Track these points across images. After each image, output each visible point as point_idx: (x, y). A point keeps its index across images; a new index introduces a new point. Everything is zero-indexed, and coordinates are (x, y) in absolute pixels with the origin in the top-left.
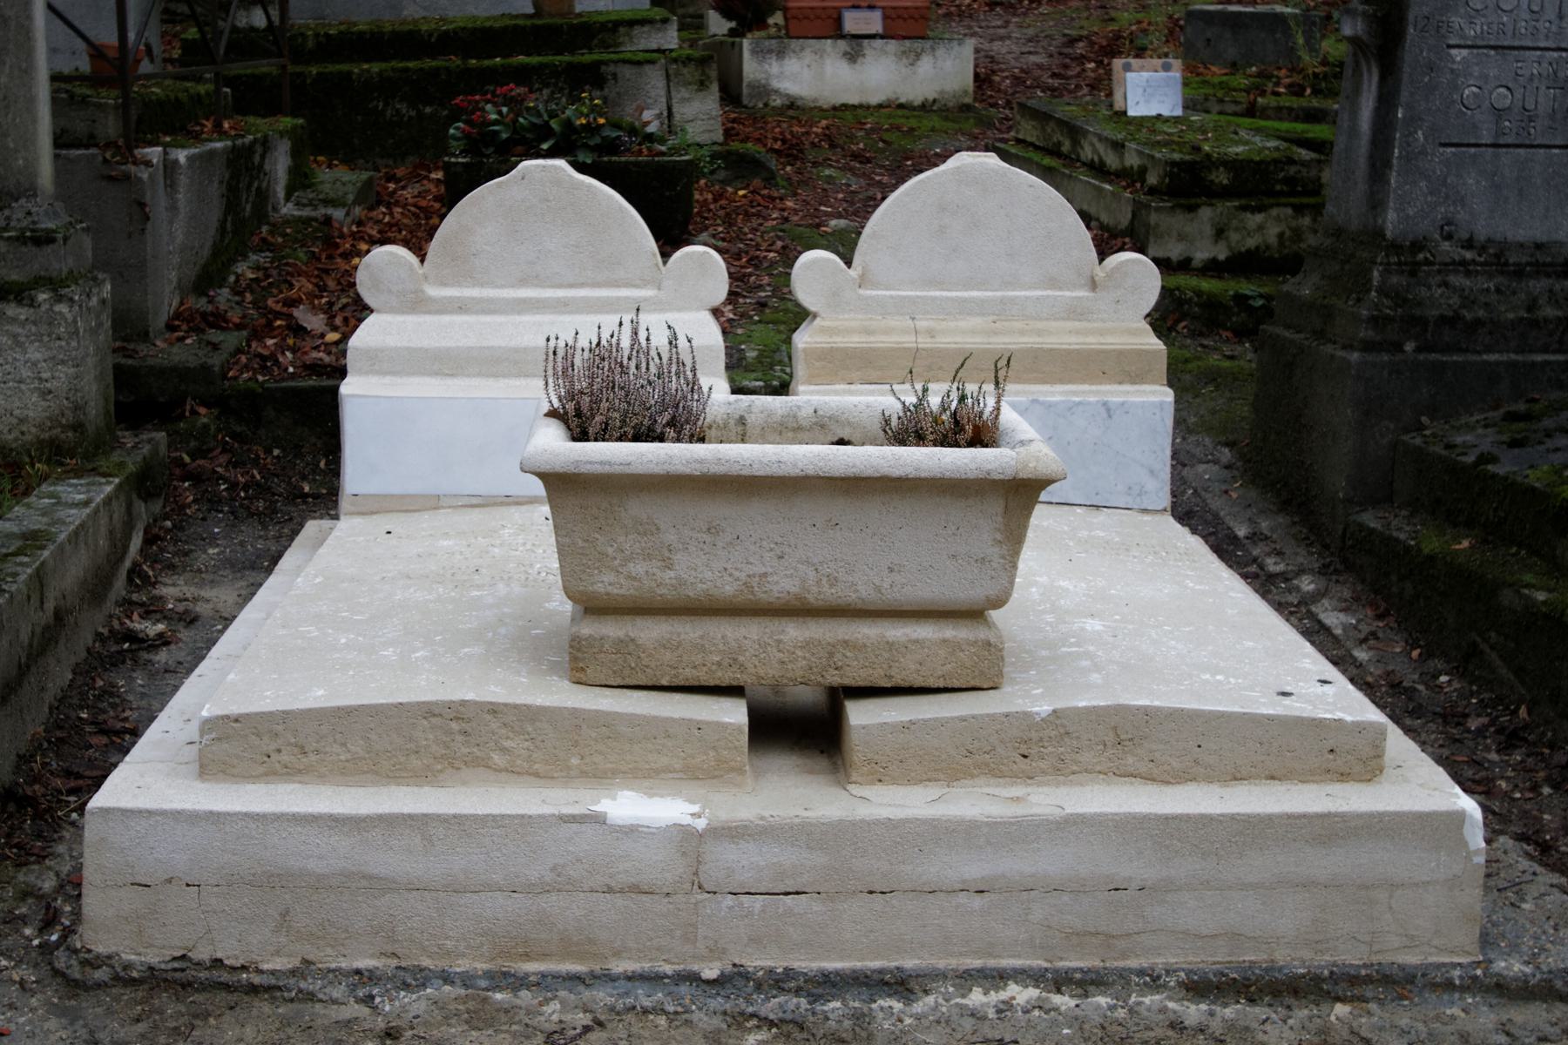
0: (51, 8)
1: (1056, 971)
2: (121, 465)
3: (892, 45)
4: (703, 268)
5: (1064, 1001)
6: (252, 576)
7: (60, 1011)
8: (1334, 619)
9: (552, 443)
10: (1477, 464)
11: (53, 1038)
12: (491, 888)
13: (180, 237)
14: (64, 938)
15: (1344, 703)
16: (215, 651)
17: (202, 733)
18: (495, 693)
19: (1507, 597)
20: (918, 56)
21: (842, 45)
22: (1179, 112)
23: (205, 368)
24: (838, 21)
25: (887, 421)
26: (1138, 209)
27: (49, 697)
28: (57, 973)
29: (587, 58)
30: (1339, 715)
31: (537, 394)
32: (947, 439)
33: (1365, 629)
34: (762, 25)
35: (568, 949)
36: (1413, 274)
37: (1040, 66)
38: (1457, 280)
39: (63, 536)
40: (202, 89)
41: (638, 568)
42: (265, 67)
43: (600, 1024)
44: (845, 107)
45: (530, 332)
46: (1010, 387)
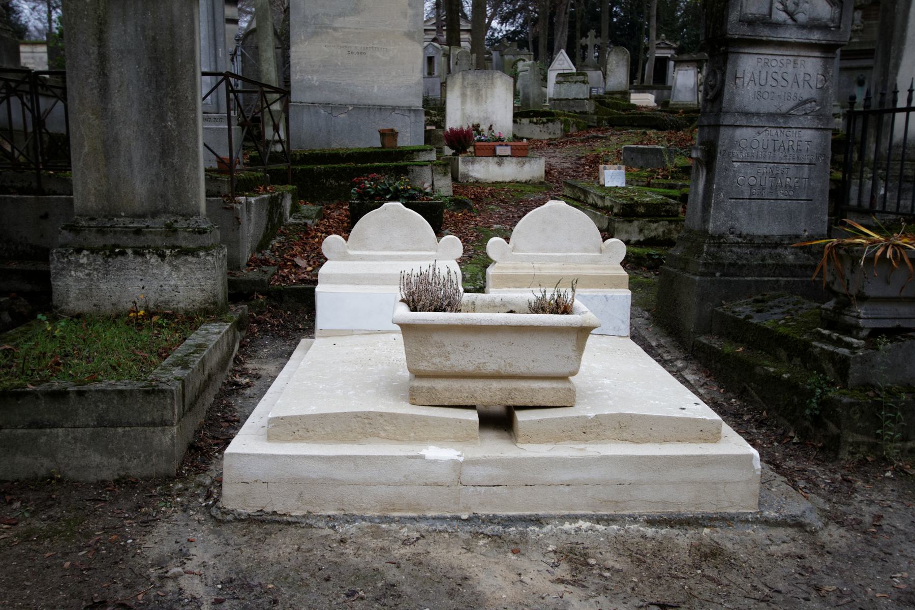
0: (205, 145)
1: (597, 515)
2: (231, 318)
3: (514, 159)
4: (453, 245)
5: (601, 527)
6: (281, 360)
7: (214, 532)
8: (690, 377)
9: (403, 312)
10: (744, 319)
11: (212, 543)
12: (380, 484)
13: (252, 231)
14: (215, 502)
15: (707, 413)
16: (270, 390)
17: (269, 423)
18: (399, 411)
19: (758, 370)
20: (524, 164)
21: (496, 159)
22: (624, 185)
23: (262, 281)
24: (494, 150)
25: (530, 304)
26: (610, 222)
27: (206, 408)
28: (212, 517)
29: (402, 163)
30: (704, 417)
31: (397, 292)
32: (554, 311)
33: (702, 381)
34: (465, 152)
35: (410, 508)
36: (719, 247)
37: (568, 168)
38: (735, 249)
39: (211, 346)
40: (259, 175)
41: (436, 360)
42: (282, 166)
43: (423, 537)
44: (497, 182)
45: (396, 268)
46: (577, 290)
